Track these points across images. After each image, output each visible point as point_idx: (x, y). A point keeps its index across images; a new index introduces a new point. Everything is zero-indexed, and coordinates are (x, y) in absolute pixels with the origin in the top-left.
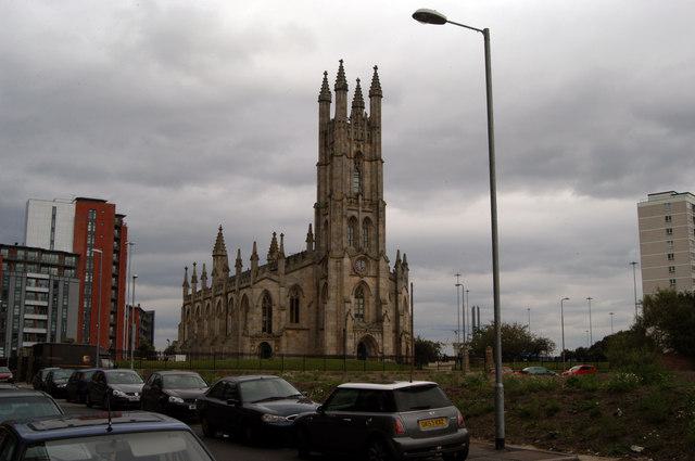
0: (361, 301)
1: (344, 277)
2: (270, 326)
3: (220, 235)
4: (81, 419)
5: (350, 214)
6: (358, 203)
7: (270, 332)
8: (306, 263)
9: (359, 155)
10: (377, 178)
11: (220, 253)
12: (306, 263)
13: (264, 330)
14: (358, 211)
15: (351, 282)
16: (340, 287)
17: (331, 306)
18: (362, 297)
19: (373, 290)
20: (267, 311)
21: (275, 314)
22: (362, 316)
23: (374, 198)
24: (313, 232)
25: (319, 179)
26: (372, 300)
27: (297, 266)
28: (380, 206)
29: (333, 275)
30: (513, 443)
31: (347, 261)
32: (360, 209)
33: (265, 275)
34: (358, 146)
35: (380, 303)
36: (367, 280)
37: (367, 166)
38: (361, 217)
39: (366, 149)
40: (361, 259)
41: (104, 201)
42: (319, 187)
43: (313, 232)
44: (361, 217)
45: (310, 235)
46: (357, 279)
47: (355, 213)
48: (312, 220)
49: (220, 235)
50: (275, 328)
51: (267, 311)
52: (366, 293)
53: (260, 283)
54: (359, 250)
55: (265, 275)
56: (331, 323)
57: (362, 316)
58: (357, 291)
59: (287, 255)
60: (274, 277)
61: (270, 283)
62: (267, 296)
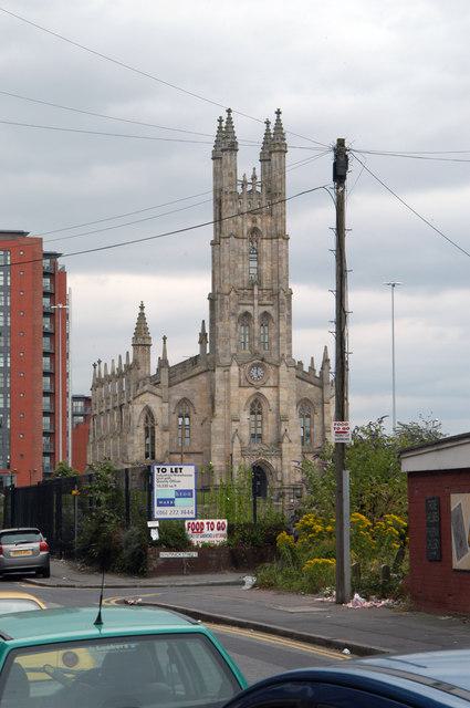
0: (259, 417)
1: (234, 393)
2: (153, 453)
3: (142, 315)
4: (281, 691)
5: (242, 309)
6: (253, 295)
7: (153, 458)
8: (197, 370)
9: (254, 231)
10: (280, 260)
11: (140, 341)
12: (197, 370)
13: (147, 456)
14: (253, 305)
15: (242, 396)
16: (228, 403)
17: (217, 425)
18: (259, 413)
19: (273, 404)
20: (150, 432)
21: (157, 436)
22: (260, 436)
23: (275, 287)
24: (207, 331)
25: (213, 261)
26: (271, 416)
27: (185, 375)
28: (282, 296)
29: (220, 388)
30: (324, 564)
31: (234, 369)
32: (256, 302)
33: (146, 388)
34: (254, 221)
35: (281, 419)
36: (264, 391)
37: (265, 245)
38: (256, 312)
39: (263, 223)
40: (258, 366)
41: (22, 234)
42: (213, 272)
43: (207, 331)
44: (256, 312)
45: (203, 335)
46: (251, 391)
47: (248, 308)
48: (205, 313)
49: (142, 315)
50: (159, 453)
51: (150, 432)
52: (264, 407)
53: (141, 398)
54: (256, 354)
55: (146, 388)
56: (218, 447)
57: (260, 436)
58: (252, 405)
59: (171, 364)
60: (157, 391)
61: (152, 397)
62: (149, 414)
